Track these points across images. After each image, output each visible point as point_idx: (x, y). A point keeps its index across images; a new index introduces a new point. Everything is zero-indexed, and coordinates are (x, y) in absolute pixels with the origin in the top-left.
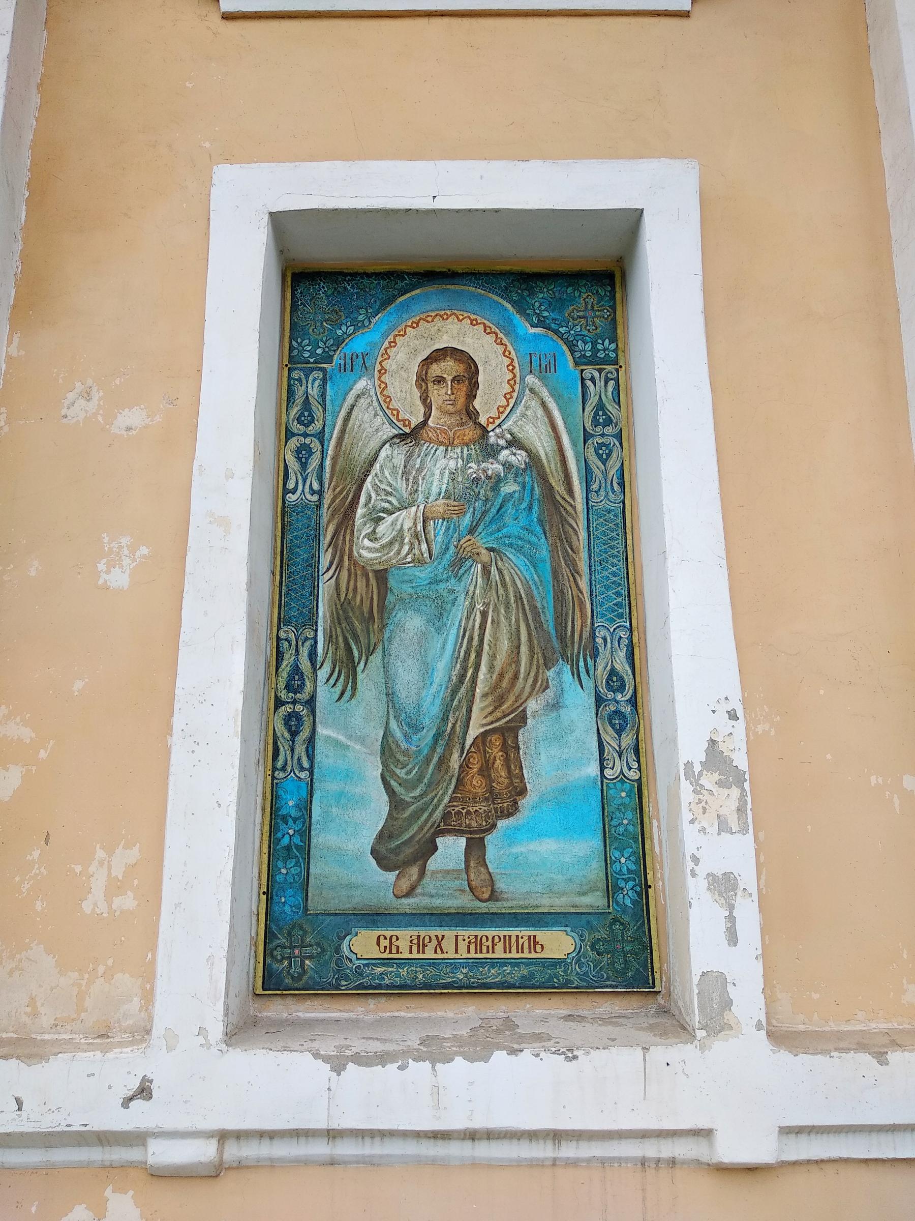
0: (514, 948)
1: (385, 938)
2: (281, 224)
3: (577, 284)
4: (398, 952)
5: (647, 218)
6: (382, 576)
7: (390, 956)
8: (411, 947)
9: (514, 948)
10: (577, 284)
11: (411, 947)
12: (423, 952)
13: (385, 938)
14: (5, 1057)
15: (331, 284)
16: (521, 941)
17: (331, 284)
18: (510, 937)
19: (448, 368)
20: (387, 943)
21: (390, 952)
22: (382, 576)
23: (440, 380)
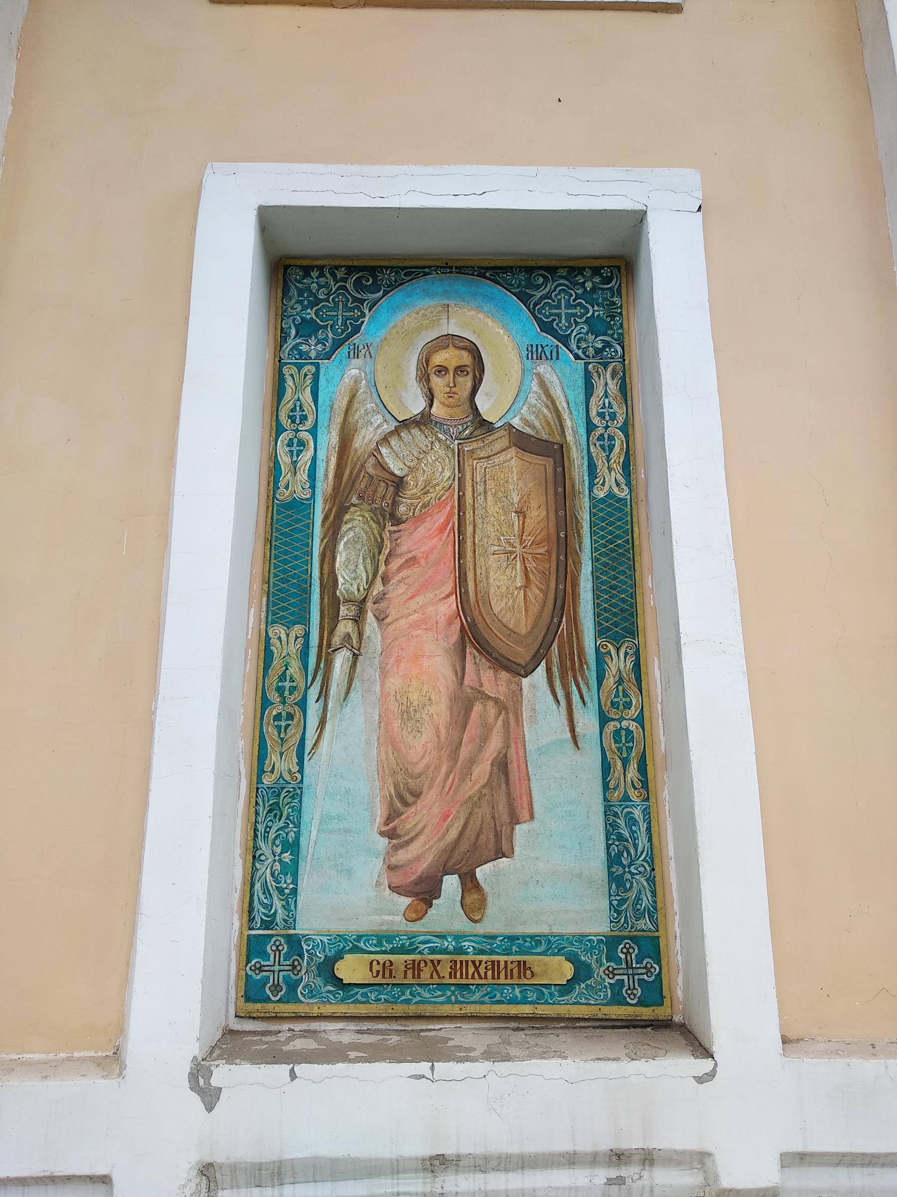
0: (502, 975)
1: (378, 963)
2: (269, 221)
3: (581, 281)
4: (390, 977)
5: (650, 216)
6: (399, 483)
7: (384, 981)
8: (406, 972)
9: (502, 975)
10: (581, 281)
11: (406, 972)
12: (419, 977)
13: (378, 963)
14: (9, 1068)
15: (322, 280)
16: (510, 966)
17: (322, 280)
18: (461, 977)
19: (446, 357)
20: (380, 968)
21: (383, 977)
22: (399, 483)
23: (442, 370)
